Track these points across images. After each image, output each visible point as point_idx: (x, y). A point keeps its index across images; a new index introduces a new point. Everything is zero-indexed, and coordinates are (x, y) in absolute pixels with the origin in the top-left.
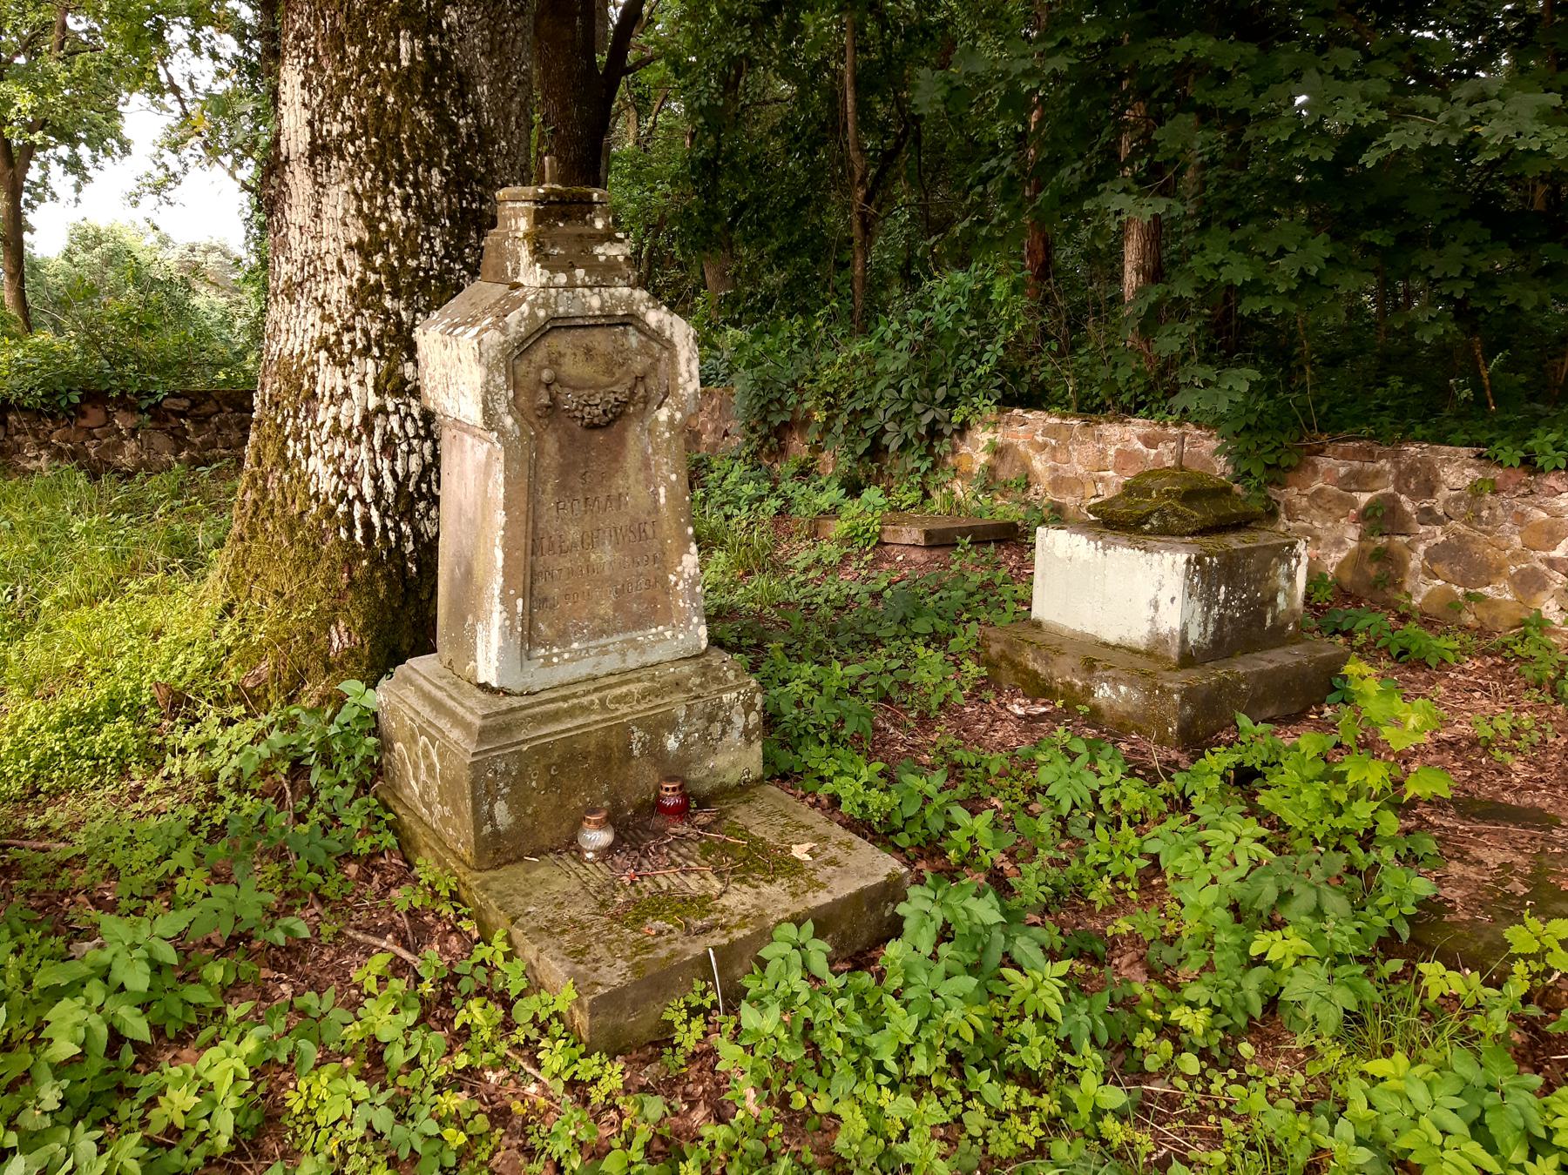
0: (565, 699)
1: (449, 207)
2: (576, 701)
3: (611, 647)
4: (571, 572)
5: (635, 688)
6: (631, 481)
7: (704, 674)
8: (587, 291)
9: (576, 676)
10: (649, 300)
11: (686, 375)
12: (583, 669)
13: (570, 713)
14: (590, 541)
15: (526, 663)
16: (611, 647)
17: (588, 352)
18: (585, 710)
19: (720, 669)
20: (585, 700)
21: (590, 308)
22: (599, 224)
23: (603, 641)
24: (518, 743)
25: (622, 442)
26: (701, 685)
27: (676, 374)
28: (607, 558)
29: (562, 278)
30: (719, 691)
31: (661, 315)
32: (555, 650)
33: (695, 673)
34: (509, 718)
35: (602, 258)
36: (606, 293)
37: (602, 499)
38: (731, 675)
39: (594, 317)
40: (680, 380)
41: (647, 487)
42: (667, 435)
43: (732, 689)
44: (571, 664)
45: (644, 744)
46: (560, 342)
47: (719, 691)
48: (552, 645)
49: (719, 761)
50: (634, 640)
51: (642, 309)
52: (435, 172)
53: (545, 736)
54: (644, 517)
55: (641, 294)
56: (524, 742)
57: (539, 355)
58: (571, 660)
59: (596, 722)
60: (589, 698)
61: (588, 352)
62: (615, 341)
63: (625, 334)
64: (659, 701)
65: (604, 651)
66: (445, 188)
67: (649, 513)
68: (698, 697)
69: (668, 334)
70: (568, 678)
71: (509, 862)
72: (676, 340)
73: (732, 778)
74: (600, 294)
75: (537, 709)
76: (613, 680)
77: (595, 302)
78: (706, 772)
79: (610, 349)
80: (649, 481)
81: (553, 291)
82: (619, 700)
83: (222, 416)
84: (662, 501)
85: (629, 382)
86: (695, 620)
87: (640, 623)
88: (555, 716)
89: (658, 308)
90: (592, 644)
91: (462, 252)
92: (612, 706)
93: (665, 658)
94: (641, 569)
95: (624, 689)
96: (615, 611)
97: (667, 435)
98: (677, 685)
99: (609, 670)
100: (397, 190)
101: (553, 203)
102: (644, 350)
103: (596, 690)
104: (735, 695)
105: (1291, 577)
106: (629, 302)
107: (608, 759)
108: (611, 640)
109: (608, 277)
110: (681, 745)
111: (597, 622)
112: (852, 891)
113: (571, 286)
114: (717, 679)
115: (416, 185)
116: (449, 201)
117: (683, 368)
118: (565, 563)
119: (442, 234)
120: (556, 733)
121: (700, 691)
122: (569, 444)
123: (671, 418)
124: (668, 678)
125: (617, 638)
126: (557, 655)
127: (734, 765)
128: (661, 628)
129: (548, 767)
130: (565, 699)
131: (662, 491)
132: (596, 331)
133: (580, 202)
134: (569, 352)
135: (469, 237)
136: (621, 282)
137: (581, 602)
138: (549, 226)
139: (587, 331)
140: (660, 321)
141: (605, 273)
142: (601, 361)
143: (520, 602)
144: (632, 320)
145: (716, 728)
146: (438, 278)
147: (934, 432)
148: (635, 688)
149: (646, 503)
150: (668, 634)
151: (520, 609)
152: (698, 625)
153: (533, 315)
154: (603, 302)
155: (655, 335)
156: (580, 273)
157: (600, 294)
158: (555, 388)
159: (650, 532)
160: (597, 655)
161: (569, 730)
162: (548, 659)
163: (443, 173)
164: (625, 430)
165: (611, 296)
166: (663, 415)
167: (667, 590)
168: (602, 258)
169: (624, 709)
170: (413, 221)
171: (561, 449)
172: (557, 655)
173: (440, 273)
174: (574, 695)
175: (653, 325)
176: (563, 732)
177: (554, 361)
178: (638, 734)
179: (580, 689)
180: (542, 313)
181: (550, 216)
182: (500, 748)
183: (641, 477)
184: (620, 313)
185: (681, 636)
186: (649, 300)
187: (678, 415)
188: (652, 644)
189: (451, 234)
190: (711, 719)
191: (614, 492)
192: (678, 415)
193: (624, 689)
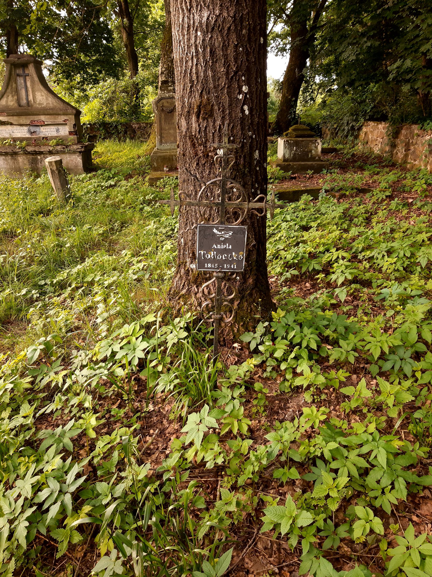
46: (163, 101)
105: (316, 147)
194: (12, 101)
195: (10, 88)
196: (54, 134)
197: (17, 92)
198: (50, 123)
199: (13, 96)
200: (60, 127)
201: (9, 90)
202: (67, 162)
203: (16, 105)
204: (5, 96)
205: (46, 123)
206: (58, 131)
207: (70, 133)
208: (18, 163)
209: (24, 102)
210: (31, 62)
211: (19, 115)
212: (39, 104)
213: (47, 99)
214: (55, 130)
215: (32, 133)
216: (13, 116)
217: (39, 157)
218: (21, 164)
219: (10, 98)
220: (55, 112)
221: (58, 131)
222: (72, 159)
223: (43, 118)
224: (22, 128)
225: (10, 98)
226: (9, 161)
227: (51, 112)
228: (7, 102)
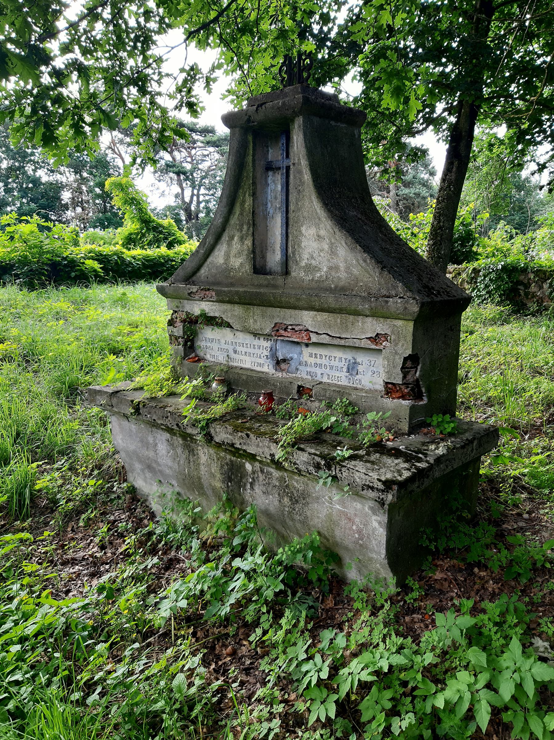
147: (353, 22)
194: (239, 254)
195: (237, 210)
196: (341, 378)
197: (256, 225)
198: (325, 339)
199: (242, 239)
200: (362, 358)
201: (234, 220)
202: (329, 517)
203: (248, 268)
204: (225, 237)
205: (314, 338)
206: (352, 368)
207: (390, 389)
208: (197, 465)
209: (275, 258)
210: (296, 114)
211: (248, 301)
212: (309, 268)
213: (333, 252)
214: (343, 365)
215: (279, 363)
216: (230, 302)
217: (248, 467)
218: (203, 470)
219: (236, 244)
220: (344, 302)
221: (352, 368)
222: (351, 512)
223: (308, 319)
224: (256, 342)
225: (236, 244)
226: (179, 450)
227: (331, 301)
228: (227, 256)
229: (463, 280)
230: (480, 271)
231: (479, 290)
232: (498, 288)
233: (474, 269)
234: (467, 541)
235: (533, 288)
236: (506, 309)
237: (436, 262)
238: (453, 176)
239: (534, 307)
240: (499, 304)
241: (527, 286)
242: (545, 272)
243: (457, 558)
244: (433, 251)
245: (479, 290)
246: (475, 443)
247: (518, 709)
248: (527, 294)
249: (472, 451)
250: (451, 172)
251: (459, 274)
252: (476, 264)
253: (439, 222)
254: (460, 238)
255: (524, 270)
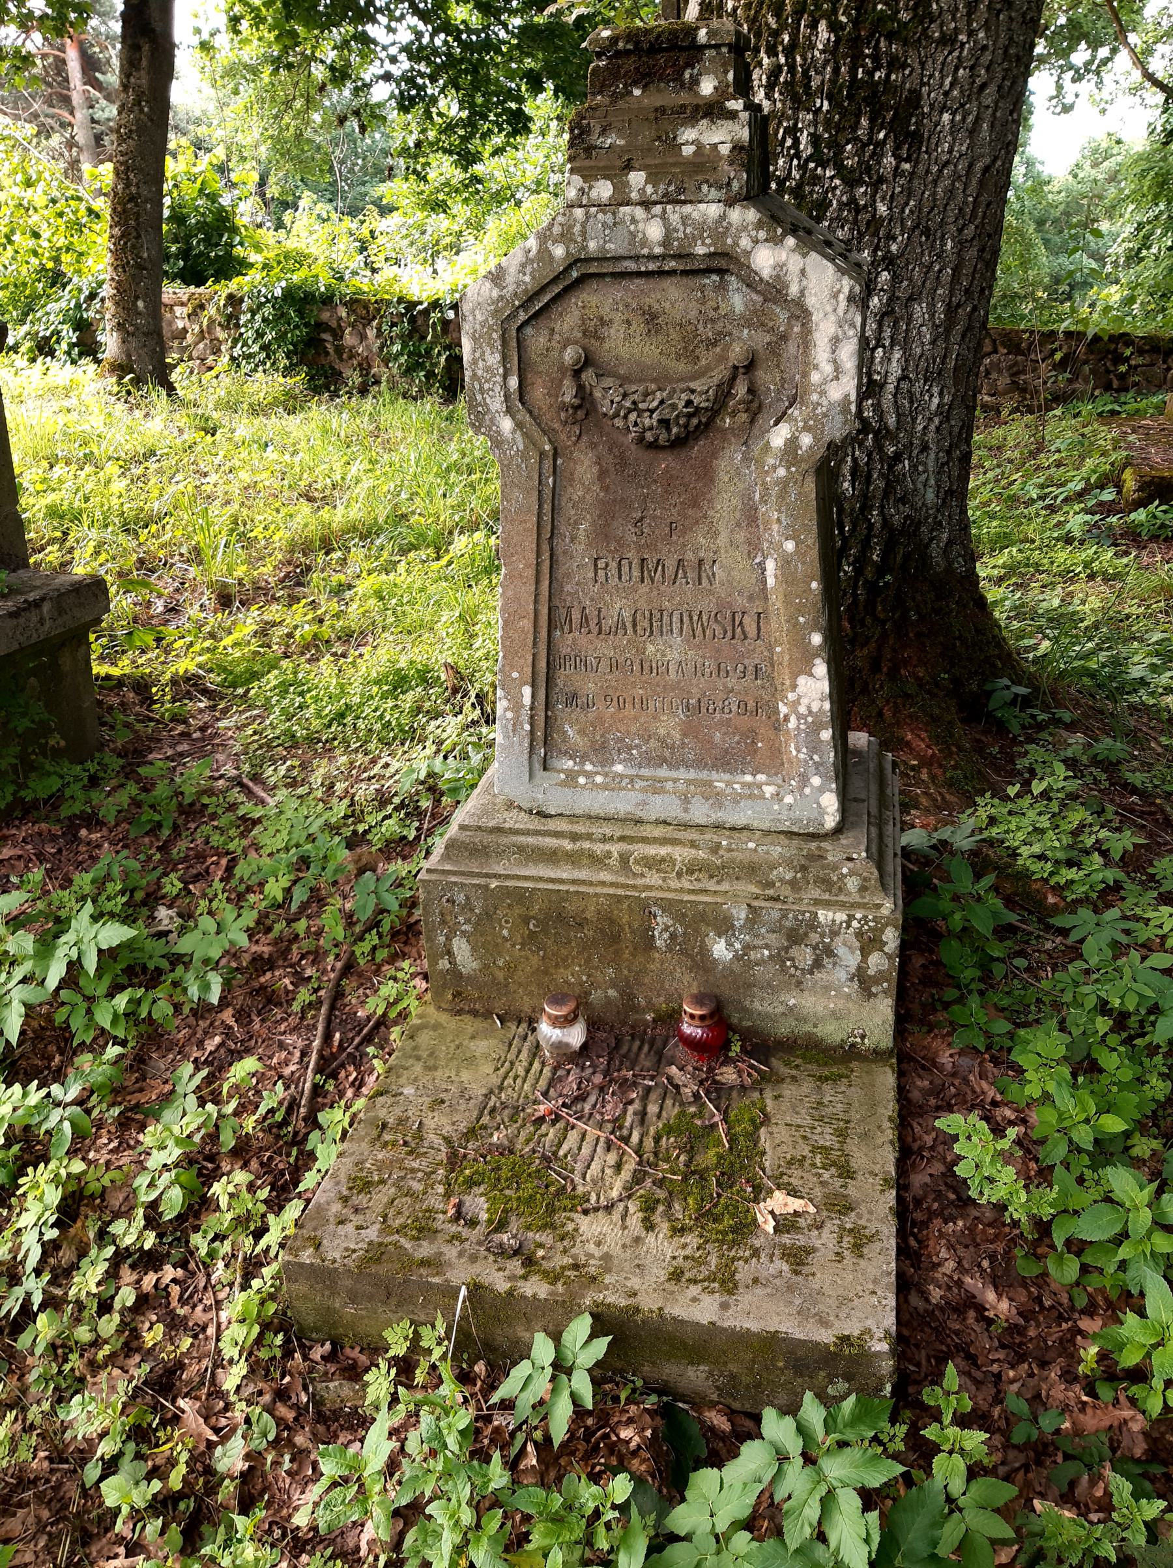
0: (574, 837)
1: (833, 81)
2: (586, 845)
3: (669, 785)
4: (614, 666)
5: (681, 854)
6: (723, 539)
7: (804, 868)
8: (639, 212)
9: (610, 810)
10: (759, 225)
11: (828, 369)
12: (623, 803)
13: (573, 858)
14: (652, 623)
15: (539, 772)
16: (669, 785)
17: (652, 319)
18: (598, 861)
19: (835, 868)
20: (599, 848)
21: (644, 242)
22: (707, 87)
23: (663, 772)
24: (487, 876)
25: (707, 474)
26: (793, 883)
27: (808, 365)
28: (673, 656)
29: (604, 190)
30: (817, 902)
31: (782, 254)
32: (589, 767)
33: (789, 863)
34: (489, 839)
35: (687, 151)
36: (674, 214)
37: (671, 564)
38: (852, 884)
39: (652, 257)
40: (815, 377)
41: (750, 556)
42: (782, 472)
43: (842, 905)
44: (593, 791)
45: (673, 936)
46: (598, 300)
47: (817, 902)
48: (584, 758)
49: (809, 1002)
50: (709, 784)
51: (745, 243)
52: (822, 26)
53: (526, 878)
54: (740, 602)
55: (744, 216)
56: (495, 876)
57: (568, 319)
58: (605, 787)
59: (603, 884)
60: (607, 847)
61: (652, 319)
62: (703, 300)
63: (722, 288)
64: (711, 885)
65: (656, 786)
66: (832, 51)
67: (751, 598)
68: (776, 899)
69: (794, 290)
70: (596, 810)
71: (474, 1013)
72: (811, 301)
73: (832, 1032)
74: (663, 216)
75: (531, 840)
76: (659, 831)
77: (654, 231)
78: (781, 1009)
79: (693, 314)
80: (754, 547)
81: (579, 213)
82: (651, 863)
83: (995, 357)
84: (771, 582)
85: (720, 374)
86: (816, 781)
87: (726, 761)
88: (552, 857)
89: (775, 241)
90: (645, 772)
91: (840, 150)
92: (637, 869)
93: (755, 824)
94: (731, 682)
95: (663, 851)
96: (685, 735)
97: (782, 472)
98: (751, 870)
99: (663, 817)
100: (766, 61)
101: (627, 53)
102: (756, 319)
103: (622, 839)
104: (841, 916)
106: (720, 229)
107: (615, 939)
108: (674, 774)
109: (690, 185)
110: (737, 958)
111: (653, 743)
112: (753, 1325)
113: (621, 199)
114: (826, 883)
115: (790, 51)
116: (836, 71)
117: (821, 354)
118: (605, 648)
119: (815, 123)
120: (541, 879)
121: (785, 891)
122: (616, 468)
123: (792, 443)
124: (738, 856)
125: (682, 774)
126: (588, 775)
127: (835, 1015)
128: (761, 777)
129: (526, 920)
130: (574, 837)
131: (770, 565)
132: (667, 283)
133: (674, 47)
134: (618, 317)
135: (856, 126)
136: (714, 194)
137: (629, 711)
138: (615, 97)
139: (652, 283)
140: (780, 266)
141: (682, 179)
142: (674, 334)
143: (527, 691)
144: (724, 264)
145: (804, 956)
146: (797, 192)
148: (681, 854)
149: (749, 580)
150: (769, 790)
151: (527, 700)
152: (821, 790)
153: (543, 254)
154: (669, 231)
155: (773, 291)
156: (637, 178)
157: (663, 216)
158: (588, 376)
159: (751, 630)
160: (643, 790)
161: (561, 881)
162: (571, 776)
163: (834, 27)
164: (714, 455)
165: (685, 220)
166: (779, 436)
167: (777, 725)
168: (687, 151)
169: (653, 878)
170: (779, 105)
171: (602, 475)
172: (588, 775)
173: (800, 185)
174: (589, 837)
175: (766, 273)
176: (552, 880)
177: (593, 331)
178: (662, 920)
179: (598, 830)
180: (559, 251)
181: (617, 78)
182: (463, 874)
183: (741, 537)
184: (700, 250)
185: (789, 799)
186: (759, 225)
187: (806, 440)
188: (737, 799)
189: (828, 123)
190: (795, 937)
191: (689, 555)
192: (806, 440)
193: (663, 851)
229: (212, 321)
230: (242, 300)
231: (245, 344)
232: (281, 338)
233: (230, 297)
234: (55, 784)
235: (349, 339)
236: (297, 382)
237: (133, 276)
238: (142, 79)
239: (355, 379)
240: (287, 372)
241: (338, 334)
242: (366, 305)
243: (47, 819)
244: (123, 249)
245: (245, 344)
246: (46, 607)
247: (78, 999)
248: (339, 350)
249: (42, 622)
250: (138, 69)
251: (202, 307)
252: (233, 285)
253: (128, 185)
254: (202, 226)
255: (327, 300)
